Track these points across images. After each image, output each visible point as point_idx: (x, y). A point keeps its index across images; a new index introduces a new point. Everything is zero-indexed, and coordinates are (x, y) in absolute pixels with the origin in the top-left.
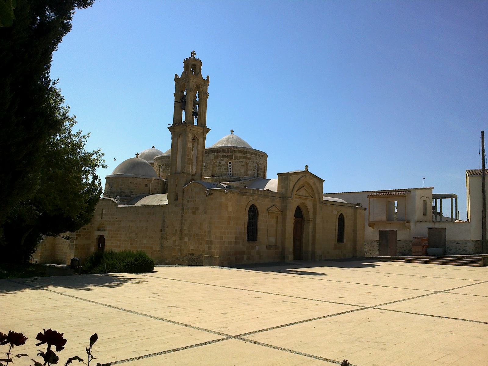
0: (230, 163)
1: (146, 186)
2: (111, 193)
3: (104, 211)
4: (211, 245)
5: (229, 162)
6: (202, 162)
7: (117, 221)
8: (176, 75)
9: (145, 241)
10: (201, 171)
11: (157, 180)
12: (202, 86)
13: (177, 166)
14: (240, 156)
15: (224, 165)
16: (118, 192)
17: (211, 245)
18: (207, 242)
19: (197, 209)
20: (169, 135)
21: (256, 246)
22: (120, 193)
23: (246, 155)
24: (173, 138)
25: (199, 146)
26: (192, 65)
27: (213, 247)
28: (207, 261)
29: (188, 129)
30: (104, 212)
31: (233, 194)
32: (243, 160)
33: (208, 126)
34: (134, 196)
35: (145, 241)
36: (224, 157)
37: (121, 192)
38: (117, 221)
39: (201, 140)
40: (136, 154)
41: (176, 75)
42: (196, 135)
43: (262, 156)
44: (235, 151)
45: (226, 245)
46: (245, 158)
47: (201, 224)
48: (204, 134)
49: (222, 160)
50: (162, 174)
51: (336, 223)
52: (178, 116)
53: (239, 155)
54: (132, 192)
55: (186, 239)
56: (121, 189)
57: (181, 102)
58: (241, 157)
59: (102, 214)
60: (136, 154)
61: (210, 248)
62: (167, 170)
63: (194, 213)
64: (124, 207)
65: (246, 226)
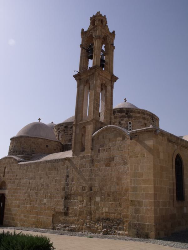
0: (130, 123)
1: (47, 146)
2: (14, 152)
3: (6, 168)
4: (139, 207)
5: (129, 122)
6: (110, 111)
7: (17, 179)
8: (83, 30)
9: (45, 201)
10: (110, 120)
11: (57, 142)
12: (108, 39)
13: (83, 114)
14: (139, 116)
15: (124, 124)
16: (20, 151)
17: (139, 207)
18: (133, 203)
19: (113, 159)
20: (75, 83)
21: (184, 207)
22: (22, 152)
23: (145, 116)
24: (78, 87)
25: (108, 94)
26: (98, 21)
27: (143, 208)
28: (134, 230)
29: (97, 73)
30: (6, 170)
31: (163, 137)
32: (143, 121)
33: (115, 74)
34: (35, 155)
35: (45, 201)
36: (123, 117)
37: (23, 151)
38: (17, 179)
39: (109, 88)
40: (38, 119)
41: (83, 30)
42: (104, 82)
43: (157, 119)
44: (135, 112)
45: (161, 207)
46: (144, 118)
47: (119, 178)
48: (112, 82)
49: (122, 120)
50: (60, 139)
51: (173, 193)
52: (84, 64)
53: (138, 115)
54: (33, 151)
55: (98, 199)
56: (23, 148)
57: (87, 50)
58: (140, 117)
59: (4, 172)
60: (38, 119)
61: (137, 211)
62: (66, 135)
63: (107, 165)
64: (25, 164)
65: (175, 181)
